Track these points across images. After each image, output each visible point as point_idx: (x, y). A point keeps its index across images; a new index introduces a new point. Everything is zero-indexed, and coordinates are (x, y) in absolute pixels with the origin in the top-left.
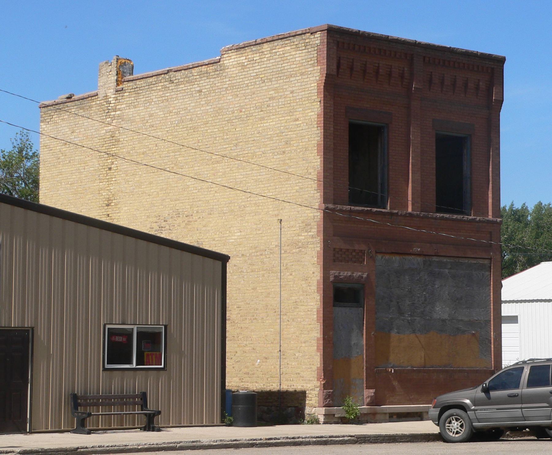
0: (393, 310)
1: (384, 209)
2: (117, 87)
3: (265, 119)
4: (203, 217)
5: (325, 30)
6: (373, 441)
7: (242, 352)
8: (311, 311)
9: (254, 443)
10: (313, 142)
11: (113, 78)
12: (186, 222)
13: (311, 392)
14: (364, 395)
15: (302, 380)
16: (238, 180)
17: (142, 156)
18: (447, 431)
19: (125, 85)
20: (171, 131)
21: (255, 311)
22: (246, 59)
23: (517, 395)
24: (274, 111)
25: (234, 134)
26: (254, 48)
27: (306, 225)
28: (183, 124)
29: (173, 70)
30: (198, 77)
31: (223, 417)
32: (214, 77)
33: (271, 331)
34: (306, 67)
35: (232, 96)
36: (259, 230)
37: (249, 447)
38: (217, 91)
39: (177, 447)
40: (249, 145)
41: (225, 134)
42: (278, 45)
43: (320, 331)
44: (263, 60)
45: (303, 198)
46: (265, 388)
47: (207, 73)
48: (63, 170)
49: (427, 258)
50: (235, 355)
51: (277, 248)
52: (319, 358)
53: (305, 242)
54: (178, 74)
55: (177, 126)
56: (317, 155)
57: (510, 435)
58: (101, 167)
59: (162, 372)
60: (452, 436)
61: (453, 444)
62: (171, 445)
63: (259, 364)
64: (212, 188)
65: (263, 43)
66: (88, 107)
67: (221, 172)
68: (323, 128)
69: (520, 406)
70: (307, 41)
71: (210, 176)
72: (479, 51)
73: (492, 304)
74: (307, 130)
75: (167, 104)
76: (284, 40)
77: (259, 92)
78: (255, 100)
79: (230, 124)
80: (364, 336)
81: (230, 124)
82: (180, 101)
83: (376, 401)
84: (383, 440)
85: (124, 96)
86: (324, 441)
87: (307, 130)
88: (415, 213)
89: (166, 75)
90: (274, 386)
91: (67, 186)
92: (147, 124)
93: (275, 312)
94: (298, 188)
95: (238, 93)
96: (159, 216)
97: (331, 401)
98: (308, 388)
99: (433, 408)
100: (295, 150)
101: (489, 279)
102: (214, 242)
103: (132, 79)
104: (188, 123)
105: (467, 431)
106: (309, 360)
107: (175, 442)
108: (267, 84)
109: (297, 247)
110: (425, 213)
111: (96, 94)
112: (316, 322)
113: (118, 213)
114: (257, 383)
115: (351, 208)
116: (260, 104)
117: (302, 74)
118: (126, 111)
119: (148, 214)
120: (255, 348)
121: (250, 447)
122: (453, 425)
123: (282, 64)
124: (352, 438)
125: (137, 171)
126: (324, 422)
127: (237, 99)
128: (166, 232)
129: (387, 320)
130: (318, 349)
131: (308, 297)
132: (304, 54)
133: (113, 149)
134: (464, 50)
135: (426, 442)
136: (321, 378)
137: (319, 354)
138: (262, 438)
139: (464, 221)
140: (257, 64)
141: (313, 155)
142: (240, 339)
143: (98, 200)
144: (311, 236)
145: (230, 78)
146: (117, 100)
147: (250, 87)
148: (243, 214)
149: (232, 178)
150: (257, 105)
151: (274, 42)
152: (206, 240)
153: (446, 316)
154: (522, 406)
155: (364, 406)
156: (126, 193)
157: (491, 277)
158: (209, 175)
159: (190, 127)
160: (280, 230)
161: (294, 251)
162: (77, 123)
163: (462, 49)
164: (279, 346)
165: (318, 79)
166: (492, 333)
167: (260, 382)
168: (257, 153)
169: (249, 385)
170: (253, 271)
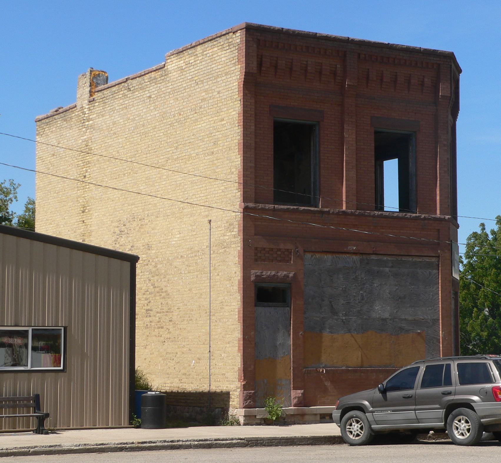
0: (325, 309)
1: (316, 207)
2: (90, 97)
3: (199, 121)
4: (152, 220)
5: (244, 28)
6: (267, 444)
7: (181, 353)
8: (234, 311)
9: (123, 447)
10: (235, 141)
11: (87, 89)
12: (139, 225)
13: (233, 393)
14: (292, 396)
15: (227, 381)
16: (178, 183)
17: (108, 163)
18: (348, 433)
19: (96, 96)
20: (128, 138)
21: (191, 312)
22: (184, 63)
23: (411, 396)
24: (205, 112)
25: (175, 137)
26: (190, 51)
27: (230, 225)
28: (137, 130)
29: (130, 78)
30: (148, 83)
31: (131, 419)
32: (160, 82)
33: (203, 332)
34: (230, 66)
35: (174, 99)
36: (194, 231)
37: (117, 451)
38: (162, 96)
39: (30, 452)
40: (187, 148)
41: (168, 138)
42: (208, 47)
43: (241, 331)
44: (196, 63)
45: (227, 198)
46: (198, 389)
47: (155, 79)
48: (52, 180)
49: (365, 257)
50: (176, 356)
51: (207, 249)
52: (240, 359)
53: (229, 242)
54: (135, 82)
55: (133, 132)
56: (238, 155)
57: (432, 437)
58: (78, 176)
59: (61, 374)
60: (352, 439)
61: (354, 447)
62: (23, 450)
63: (193, 365)
64: (159, 191)
65: (197, 46)
66: (69, 119)
67: (166, 175)
68: (242, 126)
69: (413, 407)
70: (230, 40)
71: (157, 180)
72: (422, 47)
73: (440, 303)
74: (231, 130)
75: (126, 112)
76: (213, 41)
77: (193, 94)
78: (191, 103)
79: (172, 127)
80: (292, 336)
81: (172, 127)
82: (135, 108)
83: (303, 402)
84: (280, 443)
85: (95, 106)
86: (207, 444)
87: (231, 130)
88: (349, 211)
89: (125, 83)
90: (204, 388)
91: (55, 195)
92: (112, 132)
93: (206, 313)
94: (223, 188)
95: (178, 96)
96: (120, 221)
97: (252, 402)
98: (231, 389)
99: (336, 409)
100: (222, 150)
101: (437, 277)
102: (160, 244)
103: (100, 90)
104: (141, 129)
105: (366, 434)
106: (232, 360)
107: (28, 448)
108: (200, 86)
109: (223, 247)
110: (361, 211)
111: (75, 106)
112: (237, 322)
113: (90, 219)
114: (192, 384)
115: (274, 206)
116: (194, 106)
117: (226, 74)
118: (97, 120)
119: (112, 219)
120: (191, 349)
121: (119, 452)
122: (461, 425)
123: (211, 66)
124: (241, 441)
125: (104, 177)
126: (244, 423)
127: (177, 103)
128: (125, 236)
129: (318, 319)
130: (239, 349)
131: (231, 297)
132: (227, 54)
133: (87, 158)
134: (405, 46)
135: (330, 444)
136: (241, 379)
137: (240, 355)
138: (135, 442)
139: (266, 210)
140: (192, 67)
141: (235, 154)
142: (180, 340)
143: (76, 207)
144: (234, 236)
145: (172, 82)
146: (90, 110)
147: (187, 90)
148: (182, 216)
149: (173, 180)
150: (192, 107)
151: (206, 44)
152: (155, 243)
153: (386, 315)
154: (416, 408)
155: (291, 407)
156: (96, 199)
157: (439, 275)
158: (156, 179)
159: (143, 133)
160: (209, 230)
161: (221, 251)
162: (62, 134)
163: (403, 45)
164: (209, 347)
165: (239, 77)
166: (441, 332)
167: (194, 383)
168: (193, 155)
169: (186, 386)
170: (189, 273)
